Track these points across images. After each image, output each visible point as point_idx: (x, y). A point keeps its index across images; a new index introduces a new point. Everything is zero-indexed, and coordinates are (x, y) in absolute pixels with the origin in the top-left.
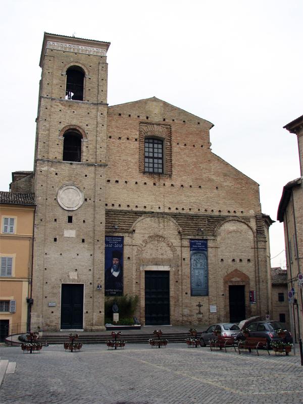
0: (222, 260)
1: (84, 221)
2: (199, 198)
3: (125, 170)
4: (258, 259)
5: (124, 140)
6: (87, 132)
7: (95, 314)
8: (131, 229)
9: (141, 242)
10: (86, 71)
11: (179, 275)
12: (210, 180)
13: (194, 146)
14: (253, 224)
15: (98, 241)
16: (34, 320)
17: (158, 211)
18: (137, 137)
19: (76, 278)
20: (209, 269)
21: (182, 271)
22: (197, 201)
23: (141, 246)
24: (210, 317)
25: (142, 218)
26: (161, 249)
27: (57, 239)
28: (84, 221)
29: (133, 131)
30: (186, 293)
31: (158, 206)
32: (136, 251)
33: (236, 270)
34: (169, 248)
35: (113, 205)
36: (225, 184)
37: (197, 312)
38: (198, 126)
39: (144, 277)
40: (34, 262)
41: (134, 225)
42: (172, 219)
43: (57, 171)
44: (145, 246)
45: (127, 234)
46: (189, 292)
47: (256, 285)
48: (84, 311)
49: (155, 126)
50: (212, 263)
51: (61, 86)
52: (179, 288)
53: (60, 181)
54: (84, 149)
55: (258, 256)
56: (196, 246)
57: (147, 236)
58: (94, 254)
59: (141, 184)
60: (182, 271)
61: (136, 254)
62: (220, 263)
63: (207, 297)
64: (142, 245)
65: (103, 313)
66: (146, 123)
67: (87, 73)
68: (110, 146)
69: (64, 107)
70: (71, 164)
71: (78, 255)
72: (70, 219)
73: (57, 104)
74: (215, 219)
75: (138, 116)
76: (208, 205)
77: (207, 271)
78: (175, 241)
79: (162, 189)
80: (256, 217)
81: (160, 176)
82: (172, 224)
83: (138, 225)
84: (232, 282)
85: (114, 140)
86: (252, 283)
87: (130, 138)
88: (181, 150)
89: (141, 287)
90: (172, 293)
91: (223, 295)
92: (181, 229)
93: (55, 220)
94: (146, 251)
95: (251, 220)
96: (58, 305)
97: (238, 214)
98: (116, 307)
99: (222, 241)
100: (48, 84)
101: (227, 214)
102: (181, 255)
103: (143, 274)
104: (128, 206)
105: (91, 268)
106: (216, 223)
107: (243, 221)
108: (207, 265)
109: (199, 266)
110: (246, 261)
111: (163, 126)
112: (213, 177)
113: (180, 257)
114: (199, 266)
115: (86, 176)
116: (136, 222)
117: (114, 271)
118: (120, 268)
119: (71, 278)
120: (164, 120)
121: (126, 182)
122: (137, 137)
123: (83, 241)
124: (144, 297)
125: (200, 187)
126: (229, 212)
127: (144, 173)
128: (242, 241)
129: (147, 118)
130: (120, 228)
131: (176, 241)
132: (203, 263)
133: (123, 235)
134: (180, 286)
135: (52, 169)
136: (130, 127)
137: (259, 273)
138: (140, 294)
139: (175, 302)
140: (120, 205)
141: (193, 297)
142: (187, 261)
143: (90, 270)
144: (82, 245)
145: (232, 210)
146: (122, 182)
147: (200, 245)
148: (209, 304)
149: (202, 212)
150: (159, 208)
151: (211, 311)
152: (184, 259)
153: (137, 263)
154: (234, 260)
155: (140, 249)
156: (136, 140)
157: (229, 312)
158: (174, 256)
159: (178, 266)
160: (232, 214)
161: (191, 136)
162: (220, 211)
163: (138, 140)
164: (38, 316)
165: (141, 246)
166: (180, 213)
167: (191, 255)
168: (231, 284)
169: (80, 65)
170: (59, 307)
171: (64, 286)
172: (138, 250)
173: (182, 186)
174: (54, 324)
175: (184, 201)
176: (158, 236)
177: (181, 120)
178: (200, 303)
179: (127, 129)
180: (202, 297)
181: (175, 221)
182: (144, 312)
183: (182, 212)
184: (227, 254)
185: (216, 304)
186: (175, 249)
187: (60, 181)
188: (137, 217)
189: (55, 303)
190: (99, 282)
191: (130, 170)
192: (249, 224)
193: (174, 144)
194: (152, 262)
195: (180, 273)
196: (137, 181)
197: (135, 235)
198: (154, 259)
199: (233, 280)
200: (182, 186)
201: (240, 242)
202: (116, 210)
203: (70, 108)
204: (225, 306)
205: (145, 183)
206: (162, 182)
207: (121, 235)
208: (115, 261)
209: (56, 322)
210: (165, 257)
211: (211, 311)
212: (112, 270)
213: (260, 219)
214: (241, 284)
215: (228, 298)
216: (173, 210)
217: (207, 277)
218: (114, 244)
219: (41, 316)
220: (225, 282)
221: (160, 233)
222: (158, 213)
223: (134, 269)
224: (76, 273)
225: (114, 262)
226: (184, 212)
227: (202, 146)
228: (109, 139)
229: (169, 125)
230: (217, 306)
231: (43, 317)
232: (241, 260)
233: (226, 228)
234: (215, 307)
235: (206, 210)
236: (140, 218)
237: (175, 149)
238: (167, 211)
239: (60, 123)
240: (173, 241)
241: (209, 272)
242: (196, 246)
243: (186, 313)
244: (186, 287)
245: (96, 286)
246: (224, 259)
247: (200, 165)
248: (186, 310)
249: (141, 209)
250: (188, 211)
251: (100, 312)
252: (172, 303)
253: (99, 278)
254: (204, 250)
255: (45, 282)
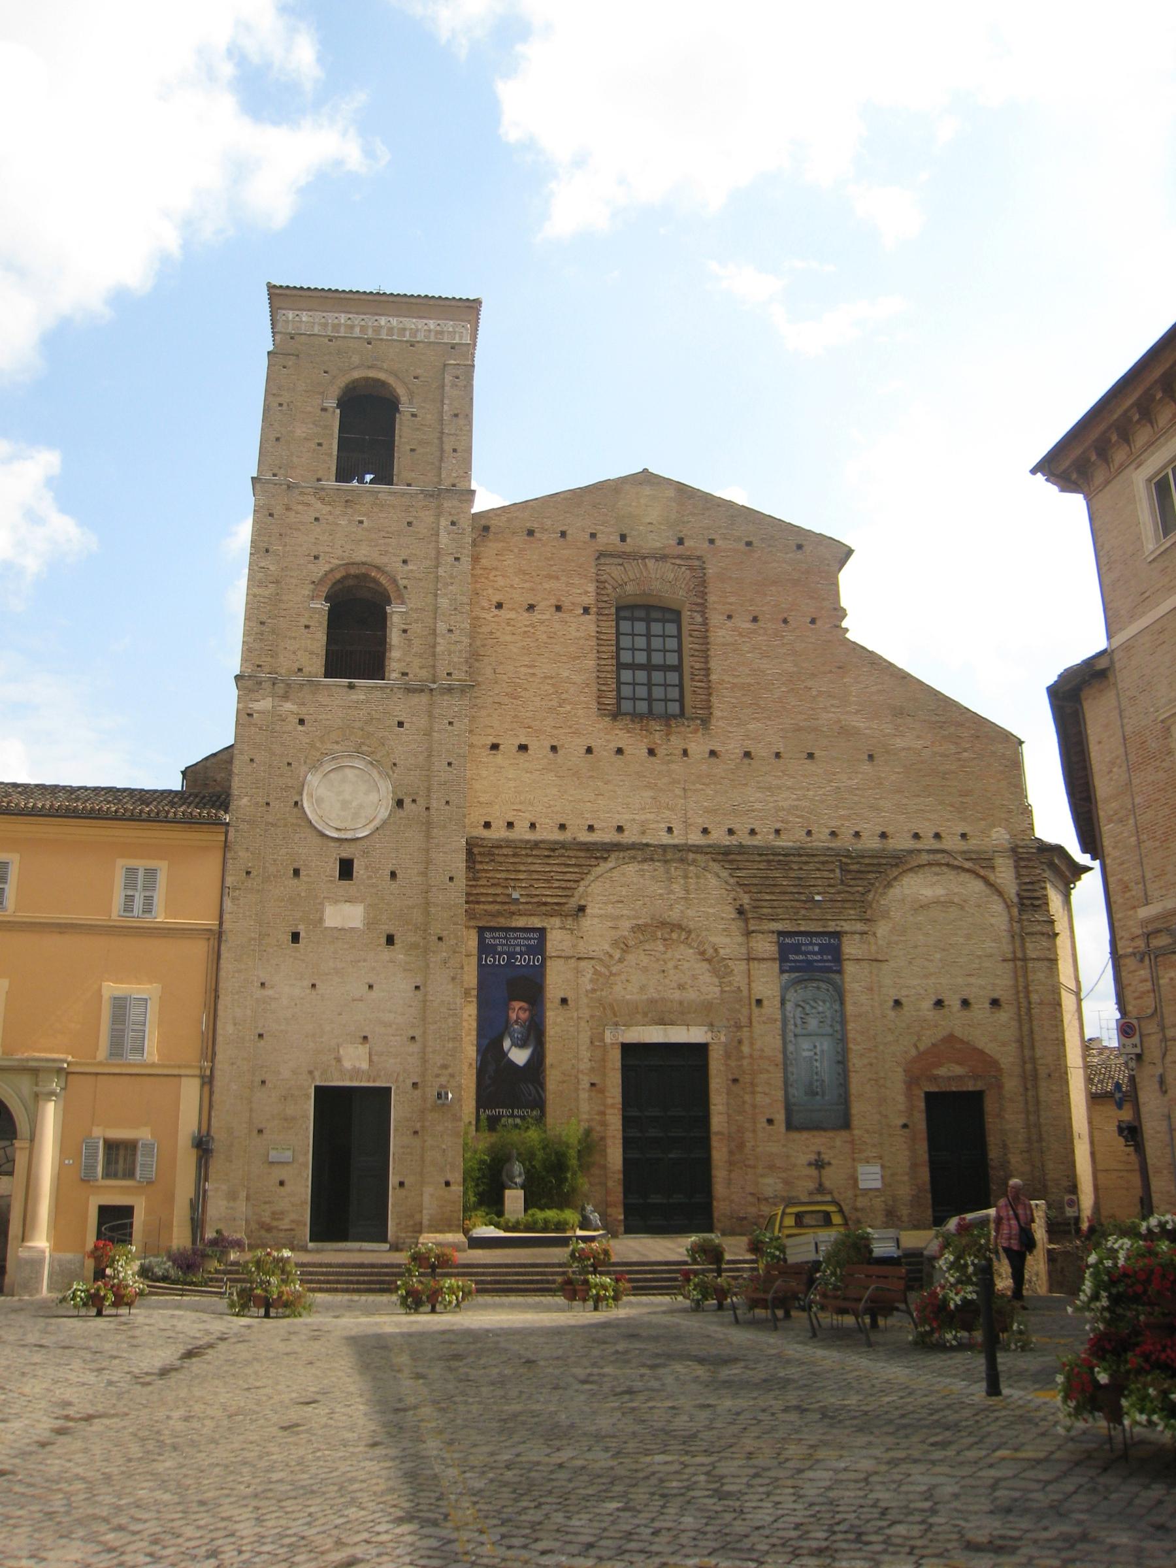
0: (897, 1003)
1: (393, 875)
2: (811, 793)
3: (551, 710)
4: (1027, 997)
5: (545, 613)
6: (405, 582)
7: (428, 1190)
8: (573, 903)
9: (607, 947)
10: (401, 391)
11: (743, 1058)
12: (845, 732)
13: (785, 621)
14: (1005, 874)
15: (440, 939)
16: (217, 1209)
17: (666, 839)
18: (589, 600)
19: (365, 1065)
20: (851, 1035)
21: (752, 1044)
22: (804, 803)
23: (606, 958)
24: (859, 1205)
25: (610, 865)
26: (676, 967)
27: (302, 935)
28: (393, 875)
29: (576, 581)
30: (770, 1121)
31: (664, 826)
32: (589, 976)
33: (950, 1039)
34: (705, 965)
35: (510, 825)
36: (899, 743)
37: (811, 1185)
38: (799, 555)
39: (618, 1065)
40: (220, 1013)
41: (581, 889)
42: (715, 867)
43: (303, 712)
44: (621, 960)
45: (556, 921)
46: (780, 1117)
47: (1027, 1089)
48: (393, 1180)
49: (651, 563)
50: (860, 1015)
51: (320, 445)
52: (744, 1102)
53: (312, 746)
54: (394, 637)
55: (1026, 987)
56: (801, 957)
57: (626, 924)
58: (425, 985)
59: (604, 752)
60: (752, 1044)
61: (589, 987)
62: (891, 1014)
63: (844, 1134)
64: (611, 956)
65: (457, 1189)
66: (620, 557)
67: (404, 399)
68: (498, 634)
69: (329, 508)
70: (351, 687)
71: (371, 987)
72: (346, 869)
73: (306, 498)
74: (867, 861)
75: (593, 535)
76: (841, 817)
77: (842, 1041)
78: (728, 940)
79: (678, 768)
80: (1014, 850)
81: (668, 725)
82: (714, 881)
83: (596, 888)
84: (935, 1078)
85: (512, 615)
86: (1011, 1085)
87: (566, 604)
88: (740, 635)
89: (610, 1101)
90: (717, 1122)
91: (905, 1126)
92: (746, 900)
93: (296, 872)
94: (623, 977)
95: (999, 861)
96: (301, 1159)
97: (951, 843)
98: (517, 1168)
99: (895, 938)
100: (278, 439)
101: (910, 844)
102: (750, 990)
103: (616, 1056)
104: (562, 827)
105: (417, 1033)
106: (871, 876)
107: (968, 865)
108: (843, 1022)
109: (813, 1023)
110: (987, 1006)
111: (678, 561)
112: (858, 722)
113: (745, 993)
114: (813, 1023)
115: (400, 724)
116: (586, 883)
117: (514, 1044)
118: (535, 1034)
119: (347, 1064)
120: (681, 542)
121: (554, 749)
122: (589, 600)
123: (390, 940)
124: (619, 1135)
125: (811, 756)
126: (916, 836)
127: (616, 715)
128: (968, 937)
129: (623, 538)
130: (535, 900)
131: (728, 943)
132: (828, 1014)
133: (545, 925)
134: (747, 1098)
135: (288, 706)
136: (563, 571)
137: (1033, 1048)
138: (604, 1124)
139: (731, 1153)
140: (533, 826)
141: (795, 1135)
142: (772, 1008)
143: (413, 1038)
144: (386, 954)
145: (927, 830)
146: (539, 748)
147: (814, 953)
148: (854, 1160)
149: (821, 839)
150: (670, 830)
151: (862, 1185)
152: (759, 1002)
153: (592, 1016)
154: (939, 1003)
155: (603, 970)
156: (586, 610)
157: (928, 1187)
158: (722, 992)
159: (739, 1027)
160: (929, 843)
161: (773, 588)
162: (883, 835)
163: (593, 610)
164: (232, 1196)
165: (606, 958)
166: (741, 846)
167: (784, 989)
168: (933, 1089)
169: (382, 376)
170: (305, 1165)
171: (323, 1094)
172: (596, 972)
173: (747, 754)
174: (285, 1224)
175: (758, 806)
176: (663, 924)
177: (739, 539)
178: (819, 1153)
179: (557, 578)
180: (831, 1134)
181: (724, 874)
182: (620, 1189)
183: (748, 841)
184: (915, 982)
185: (881, 1158)
186: (726, 966)
187: (312, 746)
188: (593, 862)
189: (289, 1153)
190: (443, 1080)
191: (568, 708)
192: (992, 878)
193: (716, 619)
194: (645, 1014)
195: (746, 1049)
196: (593, 744)
197: (586, 923)
198: (652, 1001)
199: (942, 1071)
200: (747, 754)
201: (961, 940)
202: (521, 841)
203: (350, 511)
204: (914, 1166)
205: (620, 751)
206: (676, 742)
207: (536, 922)
208: (518, 1011)
209: (293, 1216)
210: (691, 995)
211: (862, 1185)
212: (507, 1044)
213: (1029, 860)
214: (971, 1089)
215: (924, 1135)
216: (718, 836)
217: (842, 1061)
218: (511, 955)
219: (243, 1194)
220: (912, 1082)
221: (674, 915)
222: (664, 847)
223: (585, 1038)
224: (363, 1050)
225: (513, 1016)
226: (756, 843)
227: (813, 621)
228: (496, 612)
229: (699, 558)
230: (883, 1167)
231: (248, 1198)
232: (965, 1003)
233: (907, 892)
234: (877, 1169)
235: (833, 834)
236: (604, 867)
237: (721, 634)
238: (696, 838)
239: (316, 558)
240: (719, 940)
241: (851, 1046)
242: (801, 957)
243: (769, 1192)
244: (768, 1100)
245: (432, 1093)
246: (904, 1000)
247: (809, 684)
248: (769, 1180)
249: (606, 836)
250: (772, 837)
251: (447, 1184)
252: (719, 1154)
253: (445, 1067)
254: (829, 970)
255: (258, 1079)
